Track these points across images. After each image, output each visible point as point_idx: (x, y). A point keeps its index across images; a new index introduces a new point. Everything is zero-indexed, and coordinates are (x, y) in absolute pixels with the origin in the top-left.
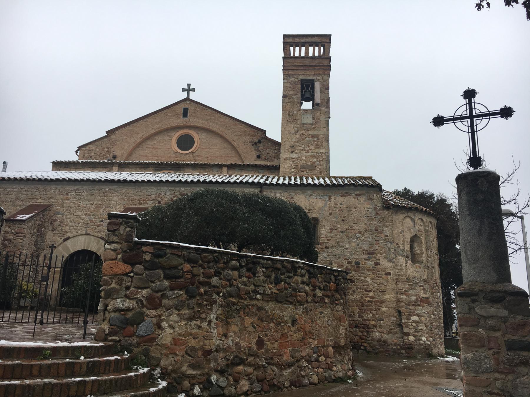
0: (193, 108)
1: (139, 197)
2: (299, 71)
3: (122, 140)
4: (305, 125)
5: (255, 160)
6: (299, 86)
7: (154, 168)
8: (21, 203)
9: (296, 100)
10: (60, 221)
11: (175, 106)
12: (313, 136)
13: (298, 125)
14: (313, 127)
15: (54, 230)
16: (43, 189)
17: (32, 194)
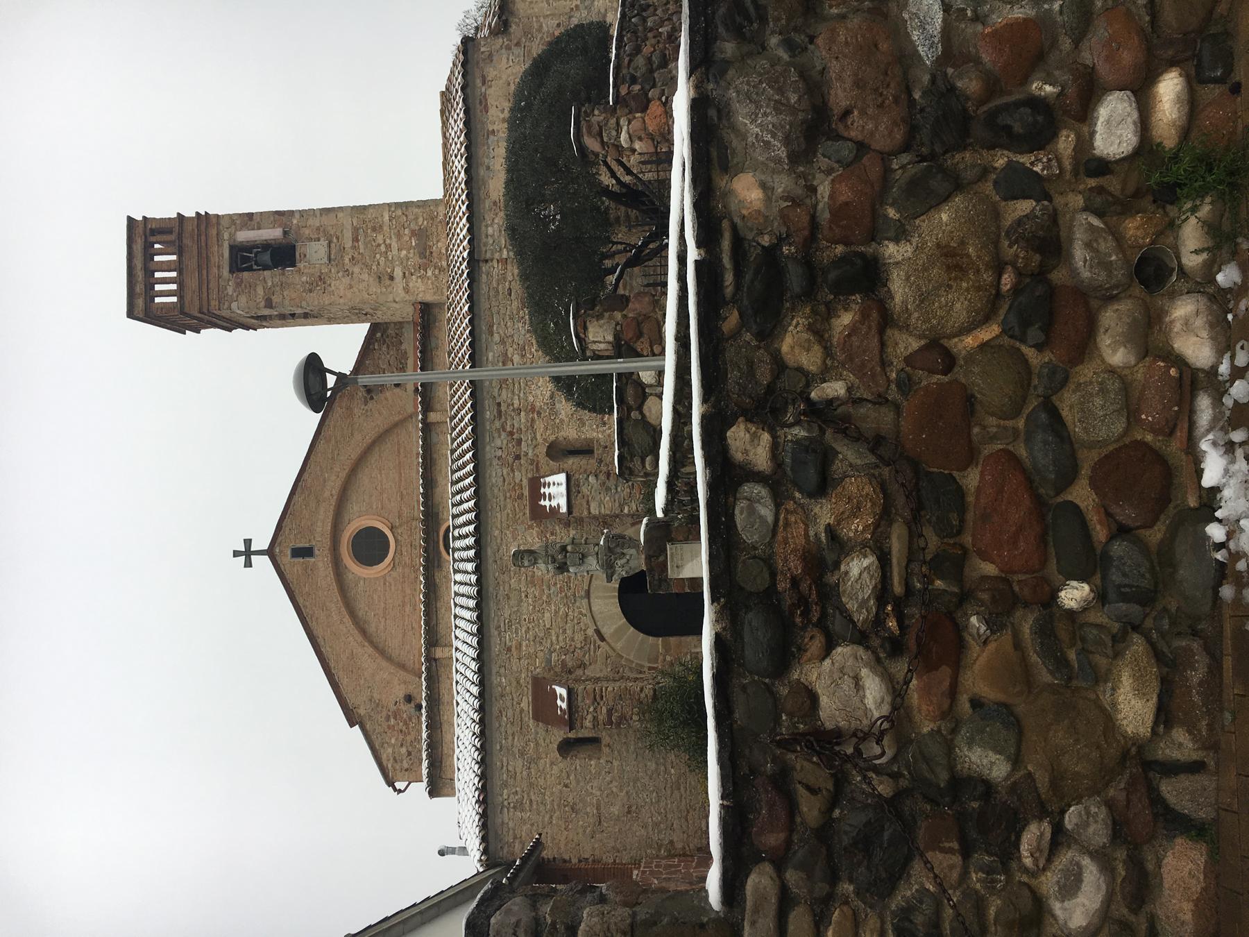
0: (292, 536)
1: (508, 500)
2: (211, 277)
3: (369, 687)
4: (332, 257)
5: (406, 391)
6: (246, 275)
7: (436, 570)
8: (532, 745)
9: (276, 280)
10: (565, 655)
11: (288, 577)
12: (356, 239)
13: (333, 270)
14: (335, 240)
15: (582, 665)
16: (501, 702)
17: (512, 723)
